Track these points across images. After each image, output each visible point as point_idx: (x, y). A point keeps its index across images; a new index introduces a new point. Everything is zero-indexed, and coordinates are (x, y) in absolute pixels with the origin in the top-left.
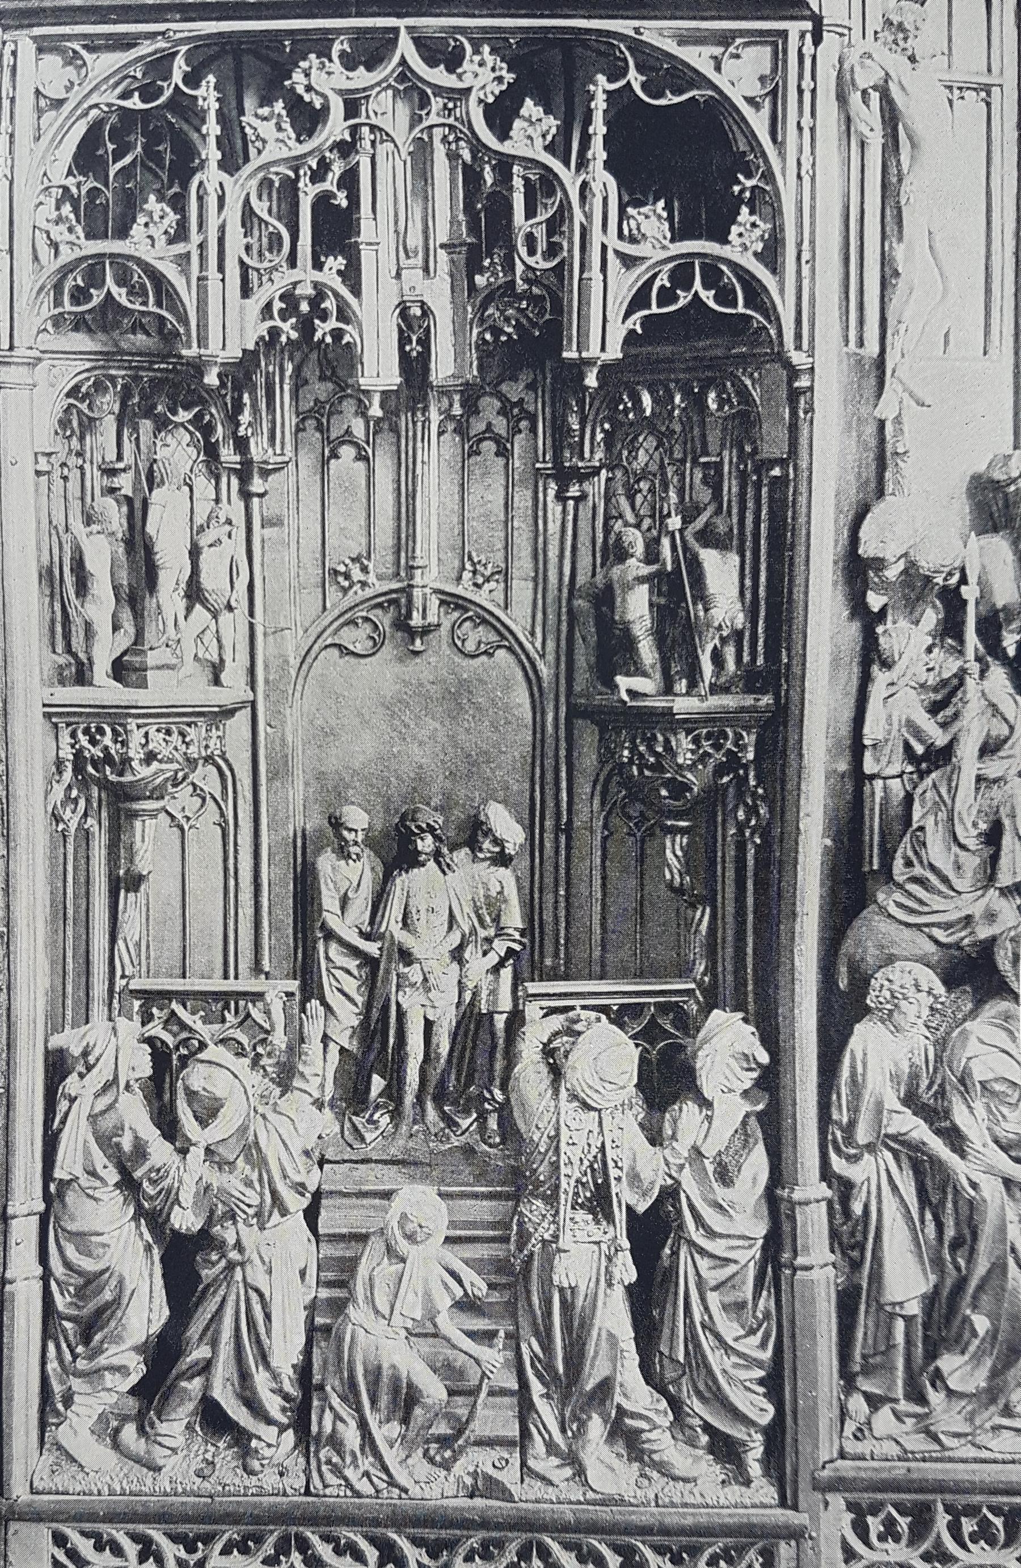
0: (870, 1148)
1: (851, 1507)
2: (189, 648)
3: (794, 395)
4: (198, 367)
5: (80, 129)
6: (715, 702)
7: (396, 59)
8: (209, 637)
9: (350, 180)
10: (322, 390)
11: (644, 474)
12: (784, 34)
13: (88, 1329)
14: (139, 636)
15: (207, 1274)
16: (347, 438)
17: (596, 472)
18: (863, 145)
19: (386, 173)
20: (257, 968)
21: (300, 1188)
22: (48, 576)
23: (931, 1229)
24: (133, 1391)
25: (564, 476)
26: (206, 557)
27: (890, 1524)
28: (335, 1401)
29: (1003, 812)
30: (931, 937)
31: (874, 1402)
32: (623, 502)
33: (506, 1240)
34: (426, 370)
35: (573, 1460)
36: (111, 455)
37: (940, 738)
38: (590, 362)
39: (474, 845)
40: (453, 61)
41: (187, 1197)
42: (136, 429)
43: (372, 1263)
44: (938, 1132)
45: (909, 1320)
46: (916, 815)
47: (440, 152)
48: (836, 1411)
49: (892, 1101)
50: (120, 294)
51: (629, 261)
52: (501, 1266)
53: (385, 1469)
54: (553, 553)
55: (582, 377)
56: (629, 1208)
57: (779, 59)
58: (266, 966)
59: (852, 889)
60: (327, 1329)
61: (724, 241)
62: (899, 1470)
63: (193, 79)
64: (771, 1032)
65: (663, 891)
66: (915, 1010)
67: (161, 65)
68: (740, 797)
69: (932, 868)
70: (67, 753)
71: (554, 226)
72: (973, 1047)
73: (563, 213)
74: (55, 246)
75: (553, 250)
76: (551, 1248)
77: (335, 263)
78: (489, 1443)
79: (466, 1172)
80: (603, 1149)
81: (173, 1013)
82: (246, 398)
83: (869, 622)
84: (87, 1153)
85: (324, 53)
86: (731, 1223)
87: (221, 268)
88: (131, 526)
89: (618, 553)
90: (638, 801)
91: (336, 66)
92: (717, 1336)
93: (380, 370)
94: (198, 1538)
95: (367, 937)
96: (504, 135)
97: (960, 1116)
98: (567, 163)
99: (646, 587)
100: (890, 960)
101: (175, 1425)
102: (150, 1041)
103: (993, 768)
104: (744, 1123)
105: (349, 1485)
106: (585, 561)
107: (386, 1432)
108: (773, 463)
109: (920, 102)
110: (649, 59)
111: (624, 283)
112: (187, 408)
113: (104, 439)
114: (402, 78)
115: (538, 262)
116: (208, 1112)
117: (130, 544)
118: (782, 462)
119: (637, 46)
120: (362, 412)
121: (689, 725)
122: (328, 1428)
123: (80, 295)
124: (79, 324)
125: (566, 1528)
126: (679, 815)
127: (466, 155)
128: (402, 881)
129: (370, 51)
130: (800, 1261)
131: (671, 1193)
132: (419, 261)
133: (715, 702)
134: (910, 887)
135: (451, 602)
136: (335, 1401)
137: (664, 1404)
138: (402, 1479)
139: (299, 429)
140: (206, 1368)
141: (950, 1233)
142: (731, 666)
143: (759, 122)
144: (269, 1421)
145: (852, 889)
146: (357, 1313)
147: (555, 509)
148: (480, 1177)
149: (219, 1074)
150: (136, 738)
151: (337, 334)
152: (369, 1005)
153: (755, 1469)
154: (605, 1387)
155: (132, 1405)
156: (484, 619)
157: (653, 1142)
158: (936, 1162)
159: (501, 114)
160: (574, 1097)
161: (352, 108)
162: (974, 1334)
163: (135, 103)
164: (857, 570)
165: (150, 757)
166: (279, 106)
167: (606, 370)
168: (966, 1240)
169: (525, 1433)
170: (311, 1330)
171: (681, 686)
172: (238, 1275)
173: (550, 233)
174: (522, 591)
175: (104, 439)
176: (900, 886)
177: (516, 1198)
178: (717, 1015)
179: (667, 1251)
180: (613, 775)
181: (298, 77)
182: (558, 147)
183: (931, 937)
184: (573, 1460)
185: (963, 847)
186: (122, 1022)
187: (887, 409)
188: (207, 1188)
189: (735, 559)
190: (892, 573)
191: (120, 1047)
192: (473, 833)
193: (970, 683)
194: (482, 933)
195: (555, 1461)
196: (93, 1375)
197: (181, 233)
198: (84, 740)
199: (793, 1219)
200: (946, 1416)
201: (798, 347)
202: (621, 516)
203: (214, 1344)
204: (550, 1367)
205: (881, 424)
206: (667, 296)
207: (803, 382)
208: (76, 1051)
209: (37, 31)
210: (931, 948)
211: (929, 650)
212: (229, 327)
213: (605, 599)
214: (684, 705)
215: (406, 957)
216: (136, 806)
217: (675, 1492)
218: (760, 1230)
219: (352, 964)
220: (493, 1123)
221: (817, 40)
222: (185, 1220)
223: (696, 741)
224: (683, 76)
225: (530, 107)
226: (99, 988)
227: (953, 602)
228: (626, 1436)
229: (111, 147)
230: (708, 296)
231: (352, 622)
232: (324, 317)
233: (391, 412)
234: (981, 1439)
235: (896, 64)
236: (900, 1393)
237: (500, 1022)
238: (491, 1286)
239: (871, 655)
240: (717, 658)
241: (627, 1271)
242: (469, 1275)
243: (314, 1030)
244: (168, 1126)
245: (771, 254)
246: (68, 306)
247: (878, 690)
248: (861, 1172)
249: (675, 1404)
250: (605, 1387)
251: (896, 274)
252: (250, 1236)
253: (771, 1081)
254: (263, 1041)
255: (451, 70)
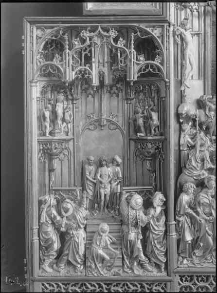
0: (183, 215)
1: (180, 276)
2: (63, 129)
3: (166, 86)
4: (65, 83)
5: (44, 43)
6: (155, 138)
7: (98, 31)
8: (66, 128)
9: (90, 51)
10: (85, 86)
11: (142, 100)
12: (164, 26)
13: (47, 248)
14: (54, 128)
15: (67, 239)
16: (90, 94)
17: (133, 99)
18: (177, 45)
19: (97, 51)
20: (75, 185)
21: (83, 224)
22: (39, 118)
23: (193, 228)
24: (55, 259)
25: (127, 99)
26: (66, 114)
27: (186, 279)
28: (90, 260)
29: (205, 156)
30: (194, 178)
31: (183, 258)
32: (138, 104)
33: (119, 232)
34: (104, 83)
35: (131, 269)
36: (50, 97)
37: (193, 143)
38: (131, 81)
39: (113, 163)
40: (108, 31)
41: (63, 226)
42: (54, 93)
43: (96, 236)
44: (194, 212)
45: (189, 244)
46: (190, 156)
47: (106, 47)
48: (177, 260)
49: (187, 207)
50: (52, 71)
51: (138, 64)
52: (120, 237)
53: (99, 271)
54: (126, 112)
55: (130, 83)
56: (141, 227)
57: (163, 30)
58: (76, 184)
59: (180, 171)
60: (88, 248)
61: (154, 61)
62: (188, 270)
63: (64, 34)
64: (166, 196)
65: (146, 170)
66: (191, 191)
67: (58, 31)
68: (159, 154)
69: (193, 166)
70: (41, 148)
71: (125, 59)
72: (201, 197)
73: (127, 56)
74: (40, 62)
75: (125, 63)
76: (128, 233)
77: (88, 65)
78: (117, 266)
79: (112, 221)
80: (136, 216)
81: (60, 194)
82: (73, 87)
83: (180, 124)
84: (46, 219)
85: (86, 30)
86: (158, 228)
87: (69, 66)
88: (53, 110)
89: (136, 112)
90: (141, 154)
91: (88, 32)
92: (157, 248)
93: (95, 82)
94: (151, 284)
95: (94, 179)
96: (117, 44)
97: (199, 210)
98: (127, 48)
99: (142, 119)
100: (186, 182)
101: (62, 265)
102: (56, 198)
103: (203, 149)
104: (161, 211)
105: (93, 274)
106: (131, 113)
107: (99, 265)
108: (163, 98)
109: (188, 35)
110: (141, 30)
111: (137, 68)
112: (63, 89)
113: (49, 95)
114: (99, 34)
115: (122, 65)
116: (67, 211)
117: (52, 112)
118: (165, 97)
119: (139, 28)
120: (93, 89)
121: (150, 141)
122: (89, 264)
123: (44, 71)
124: (45, 76)
125: (131, 281)
126: (149, 157)
127: (110, 47)
128: (100, 169)
129: (93, 30)
130: (171, 234)
131: (149, 223)
132: (102, 65)
133: (155, 138)
134: (190, 169)
135: (108, 121)
136: (90, 260)
137: (147, 259)
138: (102, 273)
139: (82, 92)
140: (68, 255)
141: (196, 229)
142: (157, 131)
143: (160, 41)
144: (79, 263)
145: (180, 171)
146: (94, 245)
147: (126, 105)
148: (115, 221)
149: (70, 205)
150: (53, 145)
151: (88, 77)
152: (95, 191)
153: (163, 270)
154: (137, 257)
155: (55, 261)
156: (114, 124)
157: (145, 215)
158: (194, 217)
159: (116, 40)
160: (131, 207)
161: (90, 39)
162: (200, 246)
163: (54, 38)
164: (178, 116)
165: (56, 148)
166: (78, 39)
167: (135, 83)
168: (199, 230)
169: (123, 264)
170: (86, 248)
171: (149, 135)
172: (73, 239)
173: (125, 60)
174: (121, 119)
175: (49, 95)
176: (188, 169)
177: (121, 225)
178: (157, 192)
179: (148, 233)
180: (137, 150)
181: (82, 34)
182: (125, 45)
183: (194, 178)
184: (131, 269)
185: (198, 162)
186: (51, 195)
187: (183, 88)
188: (67, 224)
189: (157, 113)
190: (184, 116)
191: (51, 200)
192: (113, 161)
193: (198, 135)
194: (115, 178)
195: (128, 269)
196: (48, 256)
197: (61, 60)
198: (44, 146)
199: (169, 227)
200: (196, 260)
201: (167, 78)
202: (137, 106)
203: (69, 251)
204: (128, 254)
205: (181, 91)
206: (144, 70)
207: (168, 84)
208: (44, 200)
209: (37, 25)
210: (193, 180)
211: (191, 129)
212: (70, 75)
213: (135, 120)
214: (149, 138)
215: (101, 183)
216: (54, 157)
217: (149, 274)
218: (164, 229)
219: (91, 184)
220: (117, 212)
221: (169, 27)
222: (63, 229)
223: (151, 144)
224: (147, 33)
225: (121, 39)
226: (47, 189)
227: (194, 121)
228: (141, 265)
229: (50, 46)
230: (151, 70)
231: (91, 124)
232: (86, 74)
233: (97, 90)
234: (202, 264)
235: (183, 30)
236: (188, 256)
237: (118, 194)
238: (117, 240)
239: (181, 130)
240: (155, 130)
241: (141, 237)
242: (114, 239)
243: (85, 196)
244: (60, 214)
245: (162, 64)
246: (42, 72)
247: (182, 136)
248: (182, 219)
249: (149, 259)
250: (137, 257)
251: (183, 66)
252: (75, 232)
253: (165, 204)
254: (76, 198)
255: (107, 33)
